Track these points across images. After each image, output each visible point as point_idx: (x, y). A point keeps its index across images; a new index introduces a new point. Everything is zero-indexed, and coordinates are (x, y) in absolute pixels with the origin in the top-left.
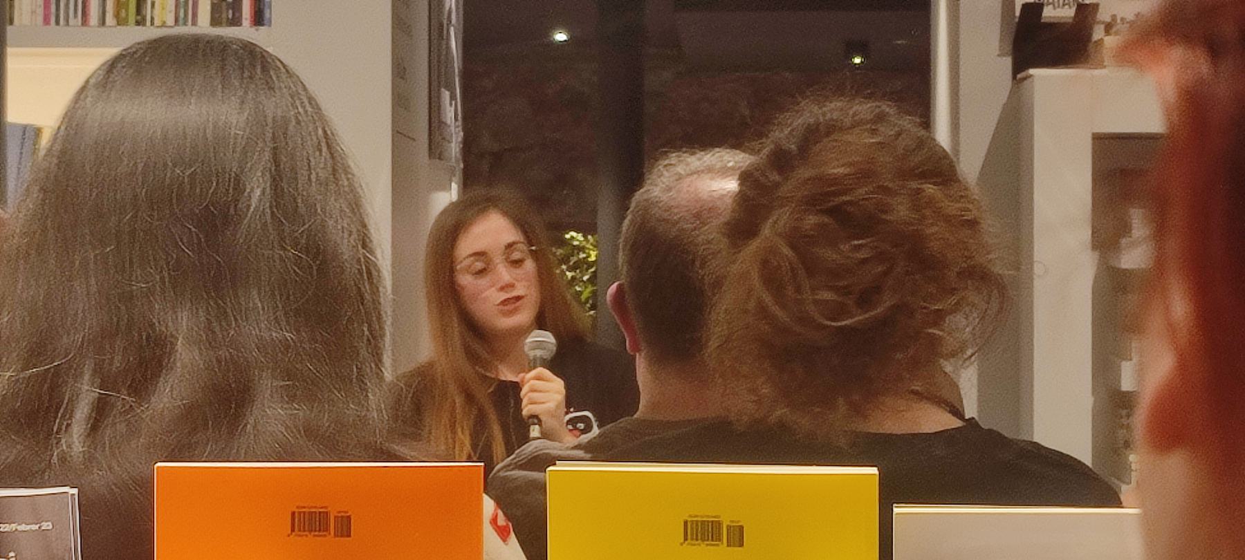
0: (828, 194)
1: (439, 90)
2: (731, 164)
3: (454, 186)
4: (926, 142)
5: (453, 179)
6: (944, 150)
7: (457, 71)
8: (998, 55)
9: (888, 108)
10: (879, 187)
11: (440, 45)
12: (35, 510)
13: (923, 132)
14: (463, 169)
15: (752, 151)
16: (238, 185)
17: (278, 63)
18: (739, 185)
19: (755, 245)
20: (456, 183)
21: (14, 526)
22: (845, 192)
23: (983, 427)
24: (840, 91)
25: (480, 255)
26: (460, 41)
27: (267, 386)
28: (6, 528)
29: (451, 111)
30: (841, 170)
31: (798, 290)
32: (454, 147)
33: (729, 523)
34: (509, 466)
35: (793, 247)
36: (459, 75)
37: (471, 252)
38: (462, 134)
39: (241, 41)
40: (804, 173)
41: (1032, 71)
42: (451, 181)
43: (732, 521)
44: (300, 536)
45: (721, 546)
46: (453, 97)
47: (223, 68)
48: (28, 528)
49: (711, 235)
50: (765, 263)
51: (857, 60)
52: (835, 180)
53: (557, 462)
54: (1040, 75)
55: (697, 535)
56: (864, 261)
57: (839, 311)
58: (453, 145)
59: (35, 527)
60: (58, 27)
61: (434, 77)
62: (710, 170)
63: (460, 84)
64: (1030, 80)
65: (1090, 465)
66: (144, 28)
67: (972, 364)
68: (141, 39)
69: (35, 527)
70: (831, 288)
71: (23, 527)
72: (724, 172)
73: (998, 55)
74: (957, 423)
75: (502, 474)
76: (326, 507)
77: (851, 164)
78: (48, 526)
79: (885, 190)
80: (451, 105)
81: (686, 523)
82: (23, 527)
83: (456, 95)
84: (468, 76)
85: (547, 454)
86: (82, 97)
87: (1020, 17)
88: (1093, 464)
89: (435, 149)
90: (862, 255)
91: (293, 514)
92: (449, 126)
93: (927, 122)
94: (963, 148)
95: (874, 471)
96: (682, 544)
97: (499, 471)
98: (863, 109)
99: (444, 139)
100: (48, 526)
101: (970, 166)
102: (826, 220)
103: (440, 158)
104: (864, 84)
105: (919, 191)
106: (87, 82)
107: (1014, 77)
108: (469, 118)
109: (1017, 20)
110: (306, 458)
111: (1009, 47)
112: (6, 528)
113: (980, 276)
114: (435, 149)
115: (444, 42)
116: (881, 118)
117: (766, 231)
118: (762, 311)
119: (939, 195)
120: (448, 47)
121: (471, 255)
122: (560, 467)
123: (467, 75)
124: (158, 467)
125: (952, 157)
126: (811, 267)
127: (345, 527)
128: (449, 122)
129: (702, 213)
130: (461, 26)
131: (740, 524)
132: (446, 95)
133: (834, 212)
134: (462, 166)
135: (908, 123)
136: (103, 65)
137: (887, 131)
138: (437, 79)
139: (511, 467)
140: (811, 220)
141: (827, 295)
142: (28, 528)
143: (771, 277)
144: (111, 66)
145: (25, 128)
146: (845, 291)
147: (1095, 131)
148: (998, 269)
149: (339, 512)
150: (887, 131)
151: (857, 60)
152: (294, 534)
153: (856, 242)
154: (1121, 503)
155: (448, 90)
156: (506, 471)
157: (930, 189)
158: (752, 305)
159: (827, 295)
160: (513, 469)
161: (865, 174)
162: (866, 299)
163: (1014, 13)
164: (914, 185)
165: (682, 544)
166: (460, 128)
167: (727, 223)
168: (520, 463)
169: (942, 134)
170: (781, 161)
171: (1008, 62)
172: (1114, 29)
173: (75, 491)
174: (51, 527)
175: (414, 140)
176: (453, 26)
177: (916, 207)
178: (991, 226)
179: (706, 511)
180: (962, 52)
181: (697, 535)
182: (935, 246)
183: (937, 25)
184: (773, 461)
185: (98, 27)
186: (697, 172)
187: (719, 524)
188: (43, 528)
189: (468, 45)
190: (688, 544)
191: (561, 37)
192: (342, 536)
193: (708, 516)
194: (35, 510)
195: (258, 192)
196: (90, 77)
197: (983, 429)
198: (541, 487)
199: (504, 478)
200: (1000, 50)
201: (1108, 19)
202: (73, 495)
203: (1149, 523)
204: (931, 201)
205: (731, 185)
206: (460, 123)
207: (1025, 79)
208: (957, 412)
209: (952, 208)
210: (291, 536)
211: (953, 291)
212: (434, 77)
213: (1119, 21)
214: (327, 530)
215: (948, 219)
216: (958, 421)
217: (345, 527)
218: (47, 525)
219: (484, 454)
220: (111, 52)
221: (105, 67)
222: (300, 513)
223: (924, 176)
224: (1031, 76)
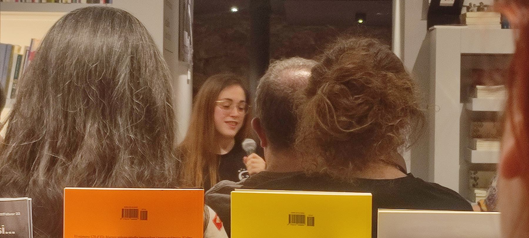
0: (343, 76)
1: (183, 32)
2: (301, 64)
3: (189, 73)
4: (390, 55)
5: (189, 69)
6: (398, 58)
7: (191, 24)
8: (422, 20)
9: (375, 41)
10: (365, 73)
11: (184, 13)
12: (13, 207)
13: (390, 51)
14: (193, 65)
15: (316, 59)
16: (115, 72)
17: (135, 19)
18: (311, 74)
19: (315, 98)
20: (190, 72)
21: (4, 214)
22: (351, 75)
23: (415, 177)
24: (354, 34)
25: (230, 100)
26: (192, 10)
27: (124, 156)
28: (1, 214)
29: (188, 41)
30: (351, 66)
31: (332, 117)
32: (189, 56)
33: (308, 216)
34: (212, 191)
35: (330, 99)
36: (192, 26)
37: (226, 97)
38: (193, 50)
39: (121, 10)
40: (336, 67)
41: (435, 27)
42: (187, 70)
43: (309, 215)
44: (126, 219)
45: (138, 220)
46: (189, 35)
47: (112, 22)
48: (10, 214)
49: (300, 94)
50: (319, 105)
51: (361, 21)
52: (348, 70)
53: (235, 189)
54: (439, 28)
55: (294, 221)
56: (360, 104)
57: (350, 126)
58: (189, 55)
59: (13, 214)
60: (21, 3)
61: (182, 27)
62: (293, 67)
63: (192, 30)
64: (434, 30)
65: (458, 192)
66: (59, 4)
67: (409, 149)
68: (78, 8)
69: (13, 214)
70: (346, 116)
71: (8, 214)
72: (304, 67)
73: (422, 20)
74: (402, 175)
75: (209, 195)
76: (137, 207)
77: (354, 63)
78: (18, 214)
79: (370, 74)
80: (188, 38)
81: (290, 215)
82: (8, 214)
83: (190, 35)
84: (195, 26)
85: (229, 186)
86: (53, 30)
87: (431, 3)
88: (459, 192)
89: (181, 56)
90: (359, 101)
91: (123, 210)
92: (187, 47)
93: (391, 48)
94: (406, 57)
95: (370, 194)
96: (288, 225)
97: (208, 193)
98: (364, 41)
99: (185, 53)
100: (18, 214)
101: (409, 65)
102: (343, 87)
103: (183, 61)
104: (364, 31)
105: (385, 75)
106: (55, 24)
107: (428, 29)
108: (196, 43)
109: (429, 5)
110: (159, 186)
111: (426, 16)
112: (1, 214)
113: (413, 112)
114: (181, 56)
115: (185, 12)
116: (370, 45)
117: (319, 92)
118: (317, 125)
119: (394, 77)
120: (187, 14)
121: (225, 99)
122: (237, 191)
123: (195, 26)
124: (66, 189)
125: (401, 60)
126: (336, 106)
127: (145, 216)
128: (187, 45)
129: (294, 85)
130: (193, 5)
131: (147, 210)
132: (186, 34)
133: (347, 84)
134: (193, 64)
135: (384, 48)
136: (63, 17)
137: (372, 51)
138: (183, 27)
139: (213, 192)
140: (338, 87)
141: (343, 119)
142: (10, 214)
143: (321, 112)
144: (66, 18)
145: (7, 46)
146: (351, 117)
147: (462, 52)
148: (421, 109)
149: (142, 209)
150: (372, 51)
151: (361, 21)
152: (290, 224)
153: (357, 96)
154: (473, 209)
155: (187, 32)
156: (211, 193)
157: (390, 74)
158: (313, 124)
159: (343, 119)
160: (214, 193)
161: (361, 67)
162: (361, 120)
163: (428, 2)
164: (384, 73)
165: (288, 225)
166: (192, 48)
167: (306, 90)
168: (217, 190)
169: (397, 51)
170: (329, 63)
171: (425, 23)
172: (470, 9)
173: (30, 199)
174: (20, 214)
175: (173, 53)
176: (190, 4)
177: (384, 82)
178: (417, 90)
179: (298, 210)
180: (406, 19)
181: (294, 221)
182: (391, 98)
183: (395, 8)
184: (286, 188)
185: (39, 3)
186: (287, 68)
187: (304, 216)
188: (16, 215)
189: (196, 13)
190: (124, 219)
191: (234, 10)
192: (143, 220)
193: (299, 213)
194: (13, 207)
195: (123, 75)
196: (57, 23)
197: (415, 178)
198: (228, 201)
199: (210, 196)
200: (422, 17)
201: (468, 5)
202: (29, 201)
203: (503, 217)
204: (390, 80)
205: (306, 74)
206: (192, 46)
207: (433, 30)
208: (404, 171)
209: (399, 83)
210: (289, 225)
211: (398, 118)
212: (182, 27)
213: (472, 6)
214: (137, 217)
215: (397, 87)
216: (404, 174)
217: (145, 216)
218: (18, 214)
219: (207, 186)
220: (65, 14)
221: (63, 19)
222: (126, 209)
223: (388, 69)
224: (435, 29)
